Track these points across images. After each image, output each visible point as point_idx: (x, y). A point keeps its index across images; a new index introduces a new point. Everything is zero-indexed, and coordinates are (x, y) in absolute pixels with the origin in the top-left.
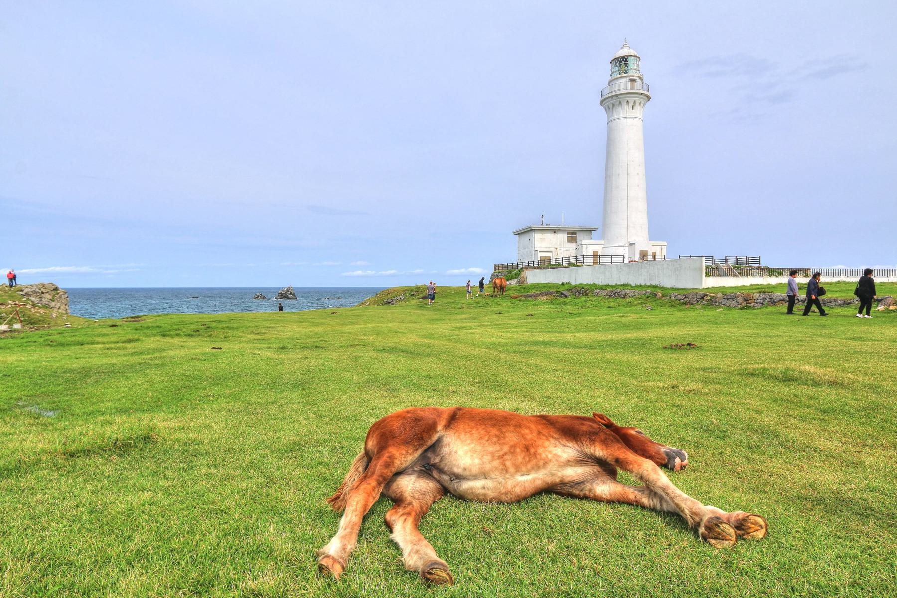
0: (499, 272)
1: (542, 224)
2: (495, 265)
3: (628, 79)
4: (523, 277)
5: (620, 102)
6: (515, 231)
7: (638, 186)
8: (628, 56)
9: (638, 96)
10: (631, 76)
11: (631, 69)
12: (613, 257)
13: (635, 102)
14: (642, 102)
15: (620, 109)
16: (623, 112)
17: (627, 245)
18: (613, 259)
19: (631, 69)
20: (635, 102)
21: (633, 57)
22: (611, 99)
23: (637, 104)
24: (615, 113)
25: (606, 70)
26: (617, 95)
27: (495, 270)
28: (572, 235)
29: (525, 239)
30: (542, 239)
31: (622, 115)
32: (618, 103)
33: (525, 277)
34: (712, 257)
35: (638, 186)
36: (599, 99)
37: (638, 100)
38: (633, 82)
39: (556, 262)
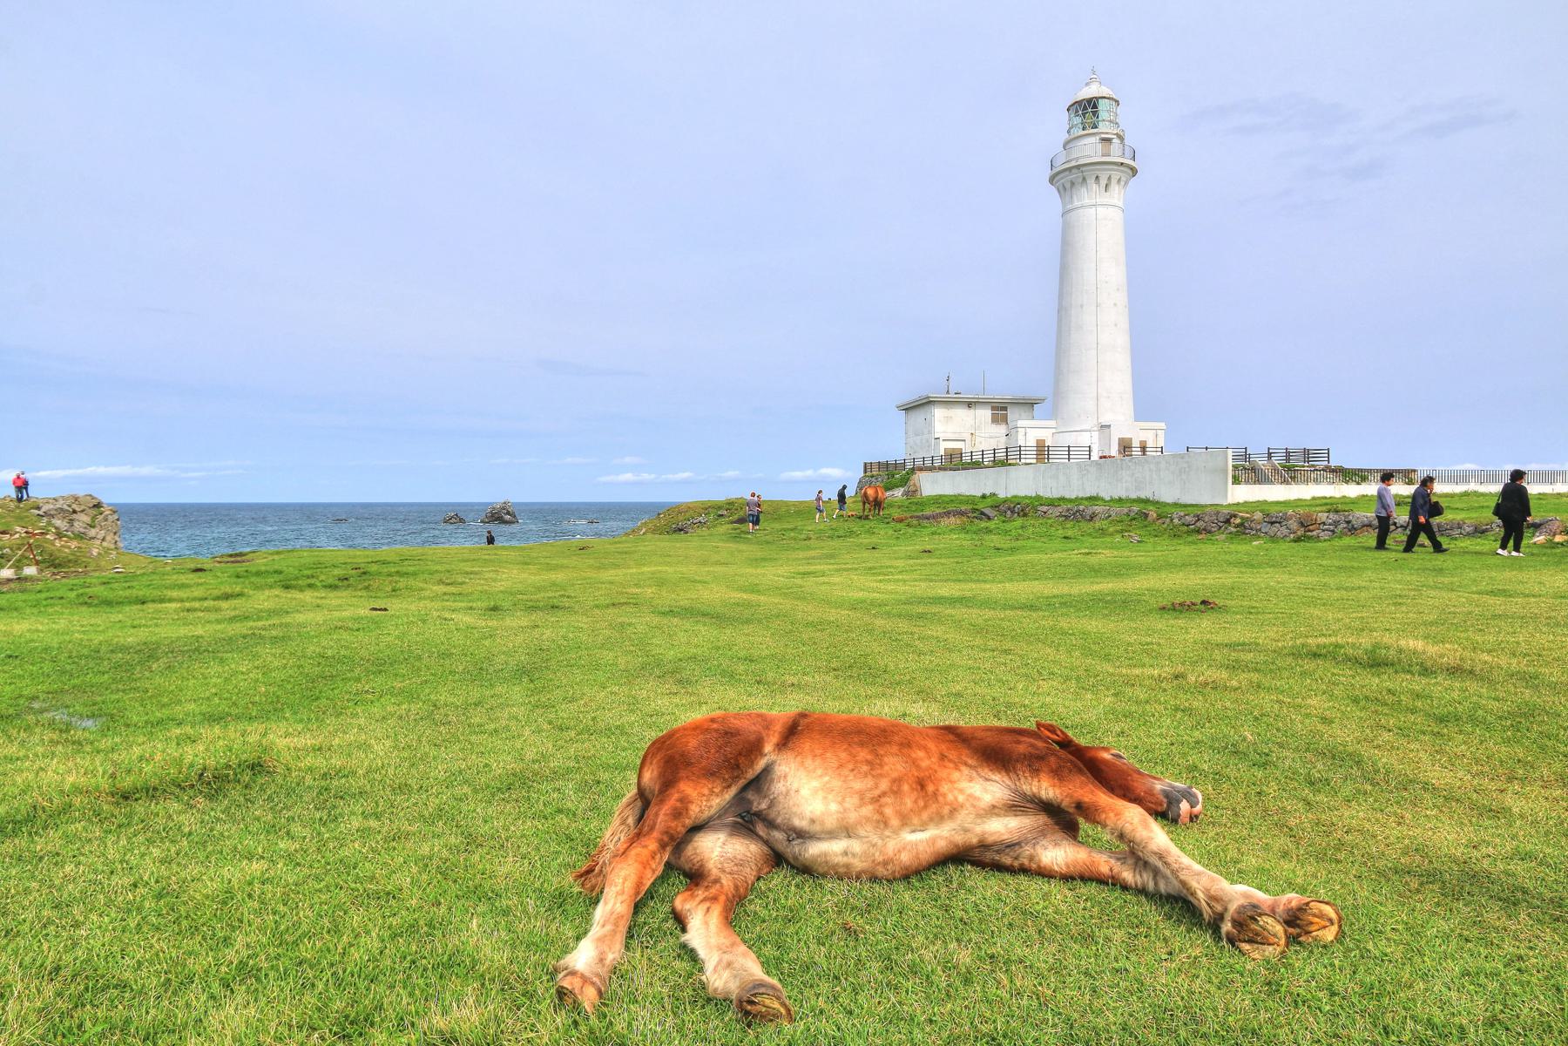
0: (872, 476)
1: (948, 392)
2: (865, 464)
3: (1098, 138)
4: (915, 485)
5: (1084, 179)
6: (899, 403)
7: (1116, 325)
8: (1097, 98)
9: (1116, 167)
10: (1103, 133)
11: (1104, 120)
12: (1071, 449)
13: (1109, 178)
14: (1122, 178)
15: (1084, 190)
16: (1089, 196)
17: (1095, 429)
18: (1071, 453)
19: (1104, 120)
20: (1109, 178)
21: (1106, 100)
22: (1067, 173)
23: (1114, 181)
24: (1075, 197)
25: (1059, 123)
26: (1078, 167)
27: (865, 472)
28: (1000, 411)
29: (918, 417)
30: (948, 419)
31: (1087, 201)
32: (1081, 180)
33: (918, 485)
34: (1244, 450)
35: (1116, 325)
36: (1048, 173)
37: (1115, 175)
38: (1107, 144)
39: (972, 459)
